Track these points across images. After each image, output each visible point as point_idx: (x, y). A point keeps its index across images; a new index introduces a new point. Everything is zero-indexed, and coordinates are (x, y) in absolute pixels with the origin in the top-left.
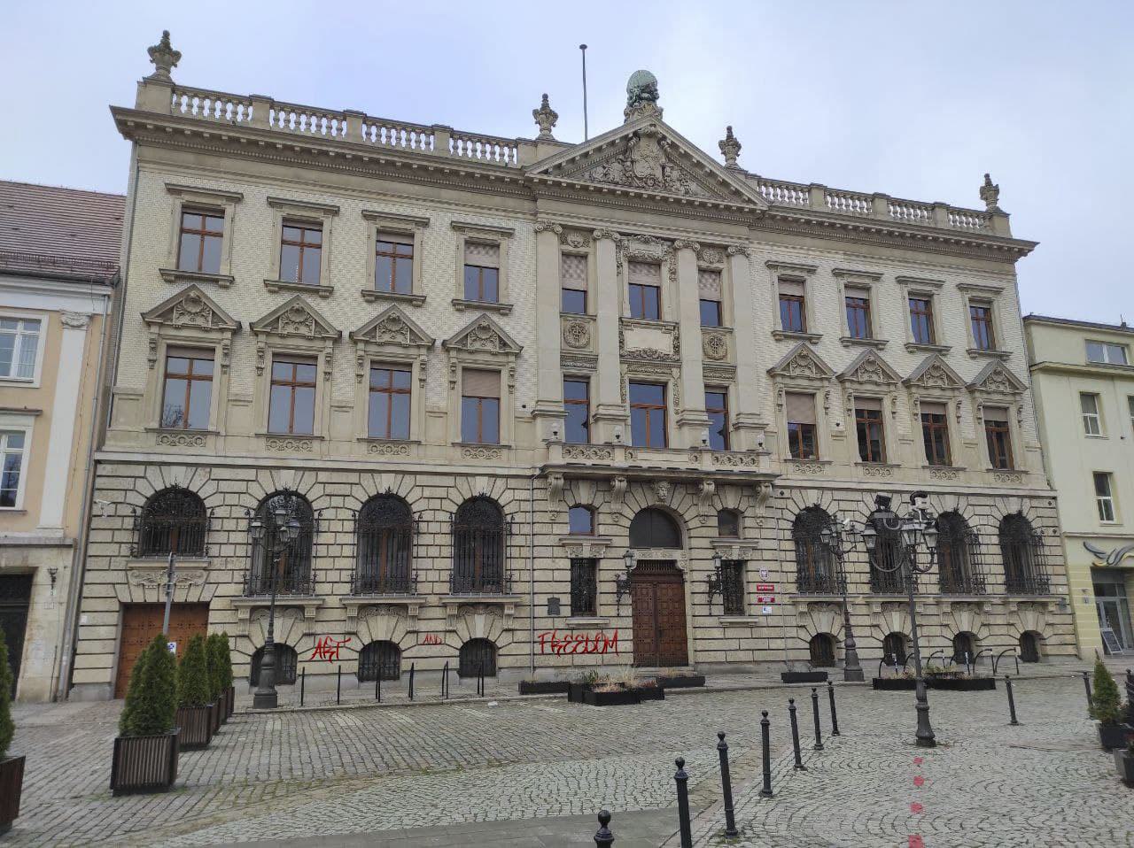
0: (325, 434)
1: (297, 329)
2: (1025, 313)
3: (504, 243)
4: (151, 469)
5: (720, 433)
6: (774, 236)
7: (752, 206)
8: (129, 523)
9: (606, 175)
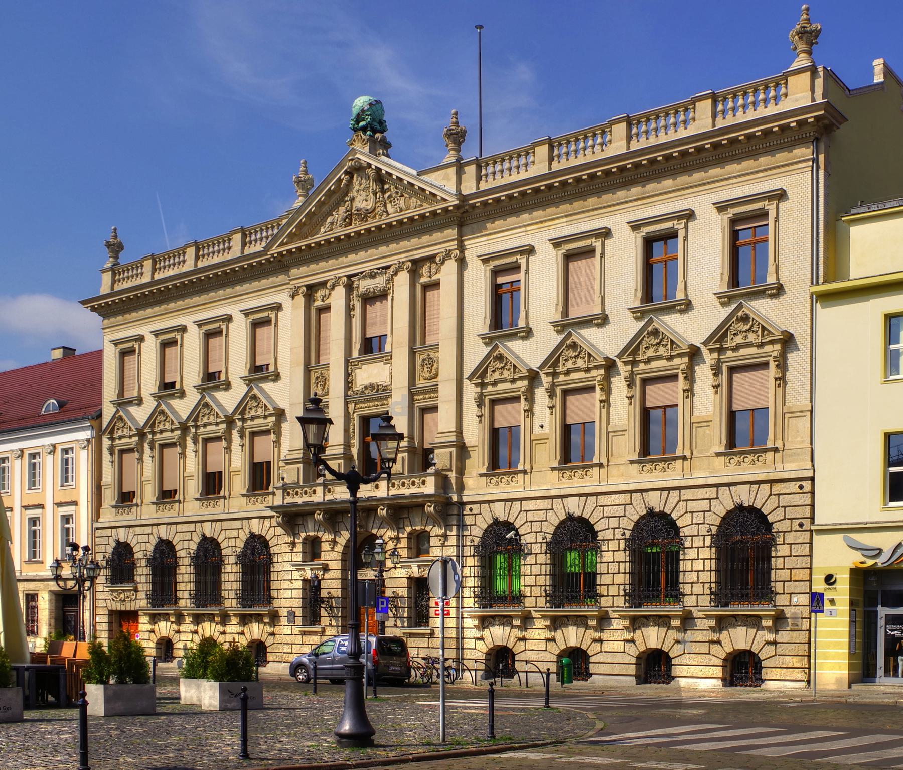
1: (575, 363)
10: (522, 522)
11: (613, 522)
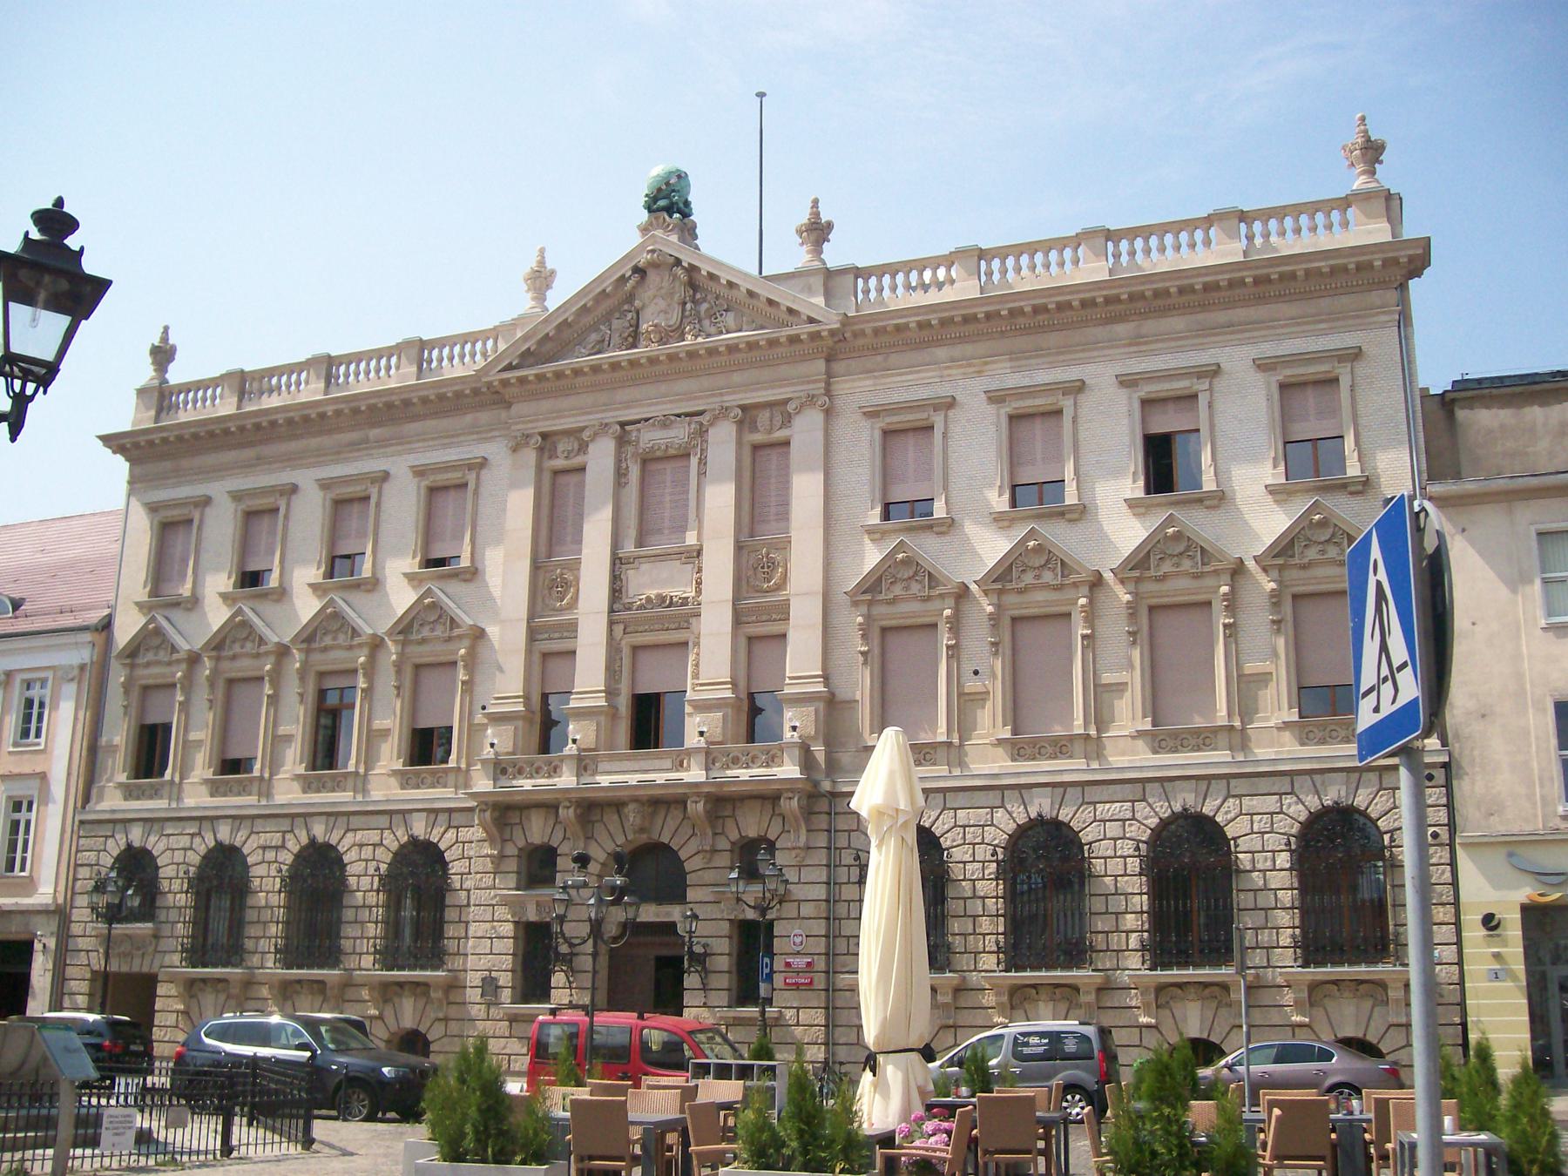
2: (1436, 377)
7: (813, 328)
10: (946, 827)
11: (1113, 829)
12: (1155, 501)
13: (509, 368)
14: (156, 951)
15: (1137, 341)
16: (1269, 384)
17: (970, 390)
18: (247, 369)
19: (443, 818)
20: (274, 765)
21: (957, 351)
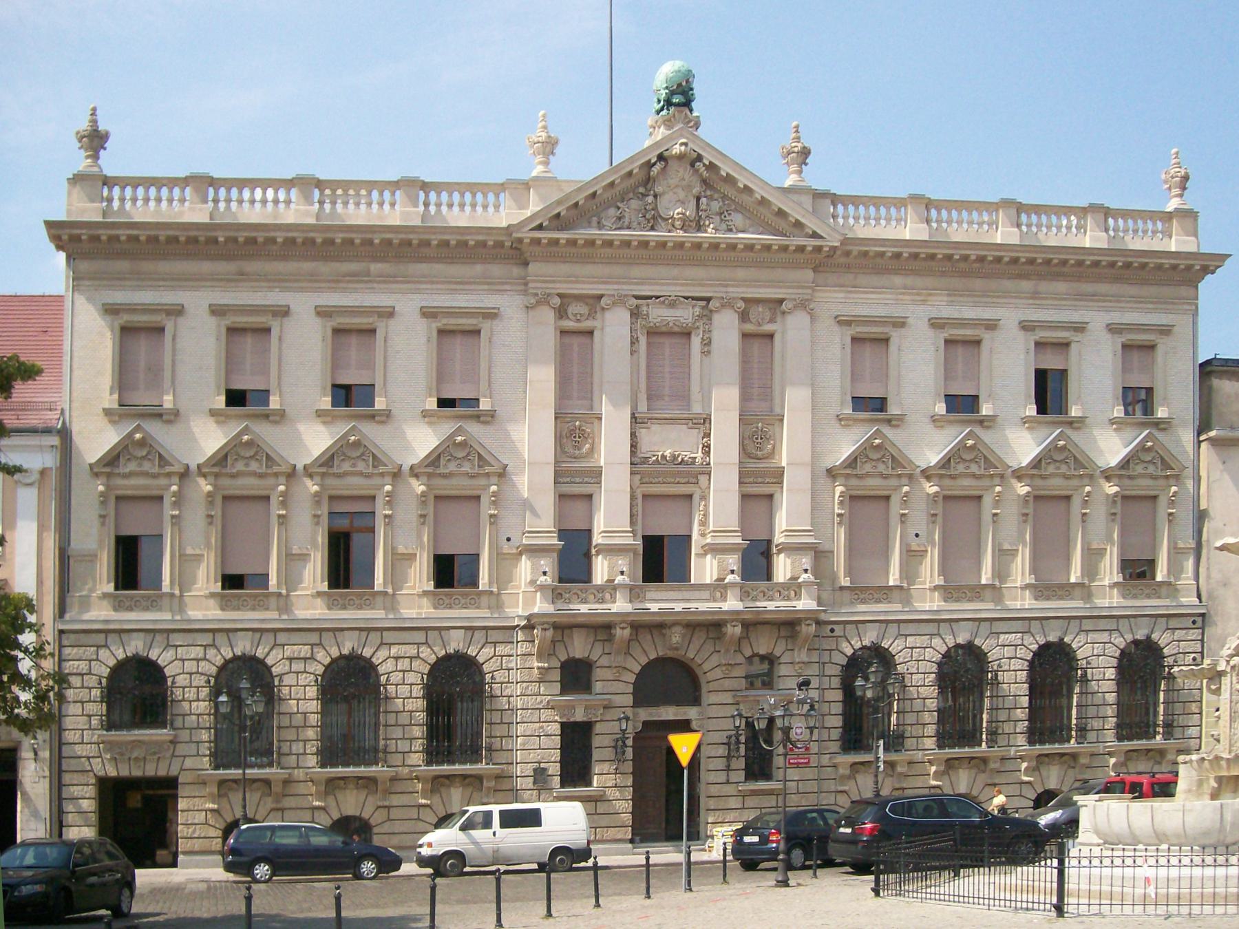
0: (824, 482)
1: (354, 465)
3: (986, 336)
4: (111, 637)
5: (762, 554)
6: (848, 278)
8: (96, 693)
9: (620, 218)
11: (190, 666)
12: (448, 414)
13: (540, 227)
14: (173, 756)
15: (1035, 295)
16: (219, 326)
17: (918, 313)
18: (1024, 202)
19: (479, 635)
20: (290, 579)
21: (909, 281)
